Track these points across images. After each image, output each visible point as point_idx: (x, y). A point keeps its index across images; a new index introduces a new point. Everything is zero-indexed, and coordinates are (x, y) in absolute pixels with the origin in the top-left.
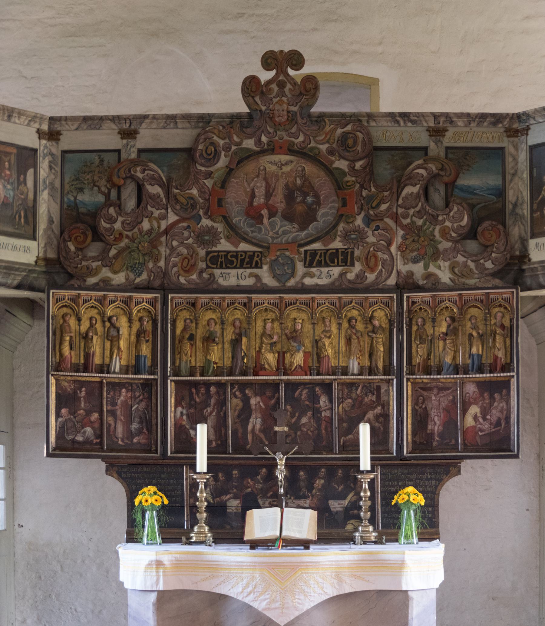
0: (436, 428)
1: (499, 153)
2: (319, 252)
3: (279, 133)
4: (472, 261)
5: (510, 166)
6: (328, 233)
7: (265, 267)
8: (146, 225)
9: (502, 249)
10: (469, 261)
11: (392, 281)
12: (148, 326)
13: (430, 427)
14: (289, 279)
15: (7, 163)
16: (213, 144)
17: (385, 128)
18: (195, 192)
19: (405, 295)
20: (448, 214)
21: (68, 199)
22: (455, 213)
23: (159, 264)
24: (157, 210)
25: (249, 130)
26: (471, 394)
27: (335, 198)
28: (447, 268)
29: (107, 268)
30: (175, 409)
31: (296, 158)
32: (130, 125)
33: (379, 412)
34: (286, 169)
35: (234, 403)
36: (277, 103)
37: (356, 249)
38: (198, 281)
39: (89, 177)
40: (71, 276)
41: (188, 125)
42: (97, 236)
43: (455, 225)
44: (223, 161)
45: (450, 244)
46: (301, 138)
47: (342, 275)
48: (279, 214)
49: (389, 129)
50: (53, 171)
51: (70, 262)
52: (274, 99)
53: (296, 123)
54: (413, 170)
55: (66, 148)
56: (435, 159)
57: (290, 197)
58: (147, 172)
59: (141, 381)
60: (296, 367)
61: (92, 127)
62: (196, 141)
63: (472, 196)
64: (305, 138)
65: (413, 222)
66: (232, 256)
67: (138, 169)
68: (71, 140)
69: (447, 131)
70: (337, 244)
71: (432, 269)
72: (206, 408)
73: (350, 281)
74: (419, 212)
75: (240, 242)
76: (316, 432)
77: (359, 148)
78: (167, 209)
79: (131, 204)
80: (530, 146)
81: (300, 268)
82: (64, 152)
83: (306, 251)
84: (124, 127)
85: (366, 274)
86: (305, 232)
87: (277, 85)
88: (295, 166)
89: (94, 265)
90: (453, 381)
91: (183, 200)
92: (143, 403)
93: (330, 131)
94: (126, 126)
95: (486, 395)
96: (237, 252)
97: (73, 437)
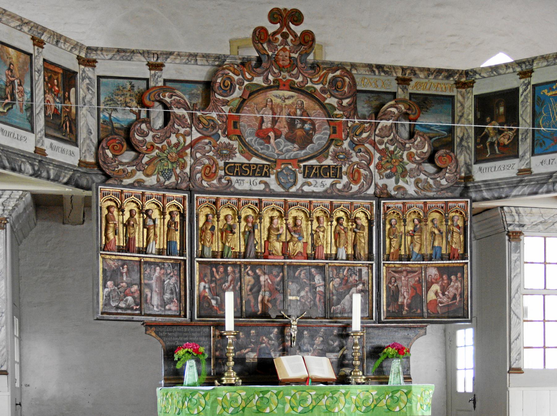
0: (405, 301)
1: (451, 99)
2: (315, 167)
3: (282, 73)
4: (431, 179)
5: (458, 110)
6: (322, 153)
7: (273, 177)
8: (173, 139)
9: (454, 170)
10: (429, 179)
11: (371, 191)
12: (177, 219)
13: (400, 300)
14: (292, 186)
15: (55, 81)
16: (230, 78)
17: (364, 76)
18: (214, 115)
19: (382, 202)
20: (413, 143)
21: (104, 115)
22: (419, 142)
23: (185, 171)
24: (183, 128)
25: (259, 70)
26: (433, 276)
27: (327, 126)
28: (413, 183)
29: (141, 172)
30: (199, 283)
31: (296, 94)
32: (157, 60)
33: (361, 288)
34: (288, 102)
35: (248, 280)
36: (281, 50)
37: (343, 166)
38: (218, 185)
39: (122, 98)
40: (108, 177)
41: (206, 63)
42: (131, 147)
43: (419, 151)
44: (237, 93)
45: (415, 165)
46: (300, 79)
47: (332, 185)
48: (283, 136)
49: (366, 77)
50: (90, 92)
51: (108, 166)
52: (278, 47)
53: (297, 66)
54: (388, 108)
55: (101, 74)
56: (403, 101)
57: (291, 124)
58: (174, 97)
59: (172, 261)
60: (298, 253)
61: (125, 58)
62: (214, 74)
63: (429, 131)
64: (303, 79)
65: (387, 148)
66: (245, 167)
67: (167, 94)
68: (105, 67)
69: (411, 80)
70: (329, 162)
71: (401, 183)
72: (224, 283)
73: (339, 190)
74: (391, 140)
75: (252, 157)
76: (312, 303)
77: (346, 89)
78: (191, 128)
79: (159, 123)
80: (475, 96)
81: (300, 179)
82: (99, 77)
83: (305, 166)
84: (152, 60)
85: (351, 185)
86: (303, 152)
87: (281, 36)
88: (295, 100)
89: (130, 169)
90: (419, 266)
91: (205, 121)
92: (173, 278)
93: (323, 75)
94: (153, 60)
95: (445, 277)
96: (250, 164)
97: (117, 304)
